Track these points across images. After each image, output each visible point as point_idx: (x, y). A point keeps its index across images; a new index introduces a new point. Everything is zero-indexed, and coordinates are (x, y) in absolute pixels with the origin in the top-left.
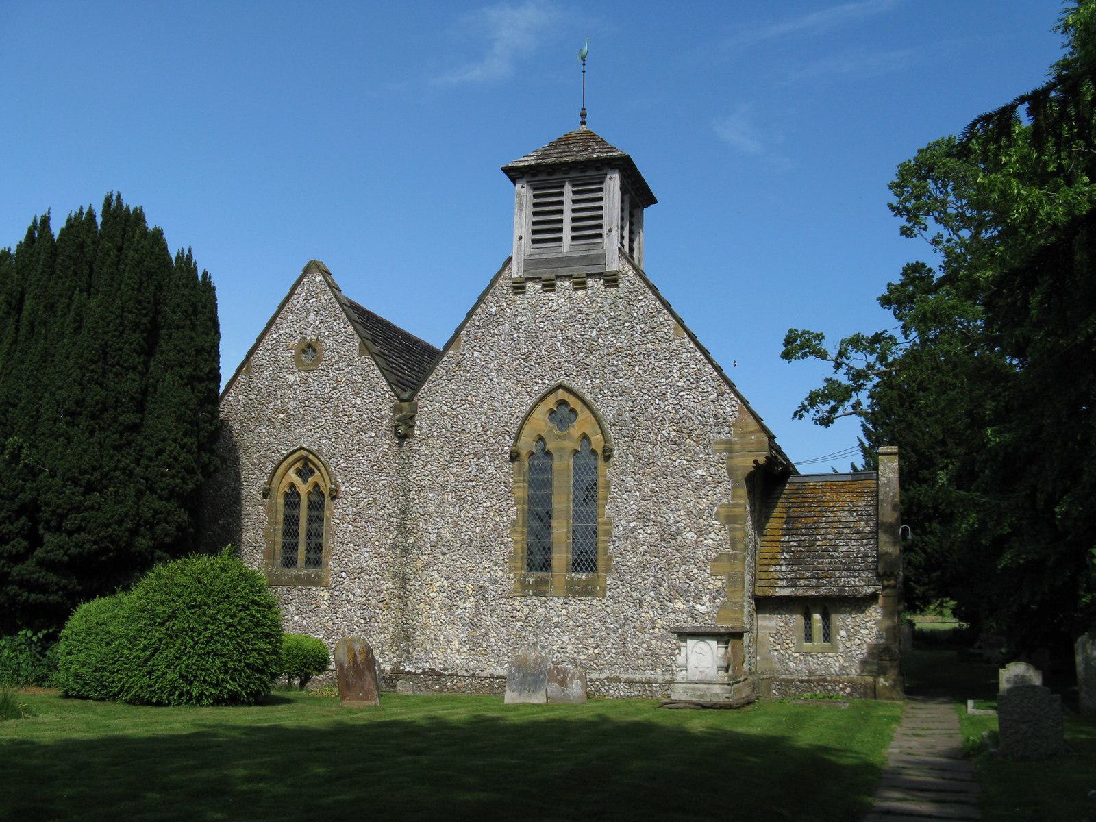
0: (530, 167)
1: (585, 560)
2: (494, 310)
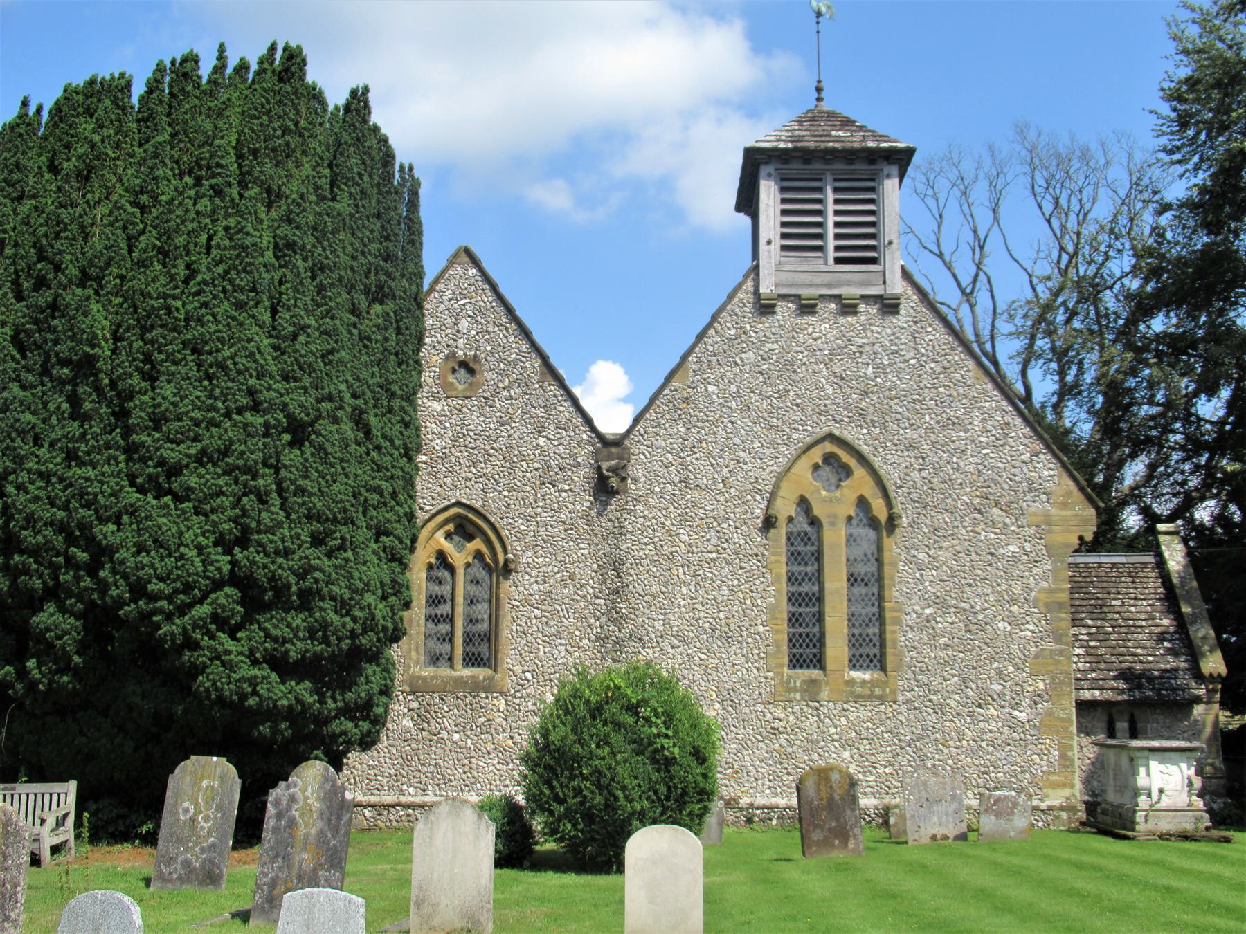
0: (785, 151)
1: (872, 650)
2: (733, 332)
